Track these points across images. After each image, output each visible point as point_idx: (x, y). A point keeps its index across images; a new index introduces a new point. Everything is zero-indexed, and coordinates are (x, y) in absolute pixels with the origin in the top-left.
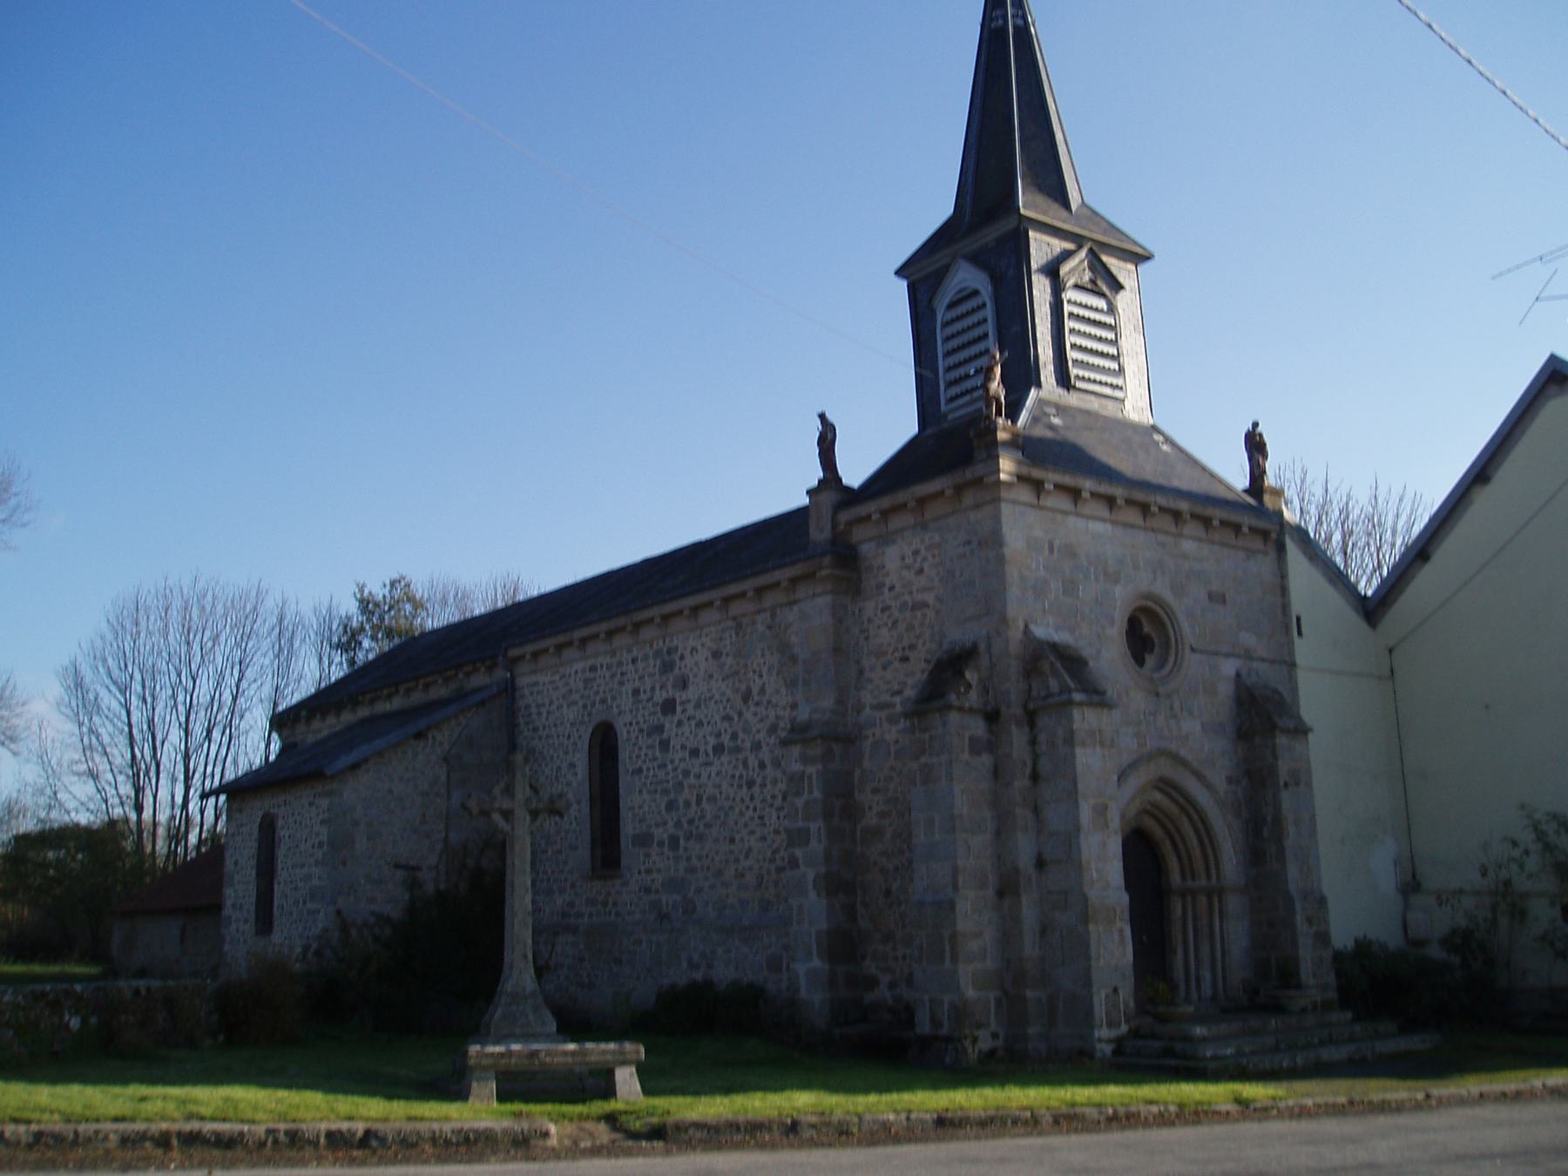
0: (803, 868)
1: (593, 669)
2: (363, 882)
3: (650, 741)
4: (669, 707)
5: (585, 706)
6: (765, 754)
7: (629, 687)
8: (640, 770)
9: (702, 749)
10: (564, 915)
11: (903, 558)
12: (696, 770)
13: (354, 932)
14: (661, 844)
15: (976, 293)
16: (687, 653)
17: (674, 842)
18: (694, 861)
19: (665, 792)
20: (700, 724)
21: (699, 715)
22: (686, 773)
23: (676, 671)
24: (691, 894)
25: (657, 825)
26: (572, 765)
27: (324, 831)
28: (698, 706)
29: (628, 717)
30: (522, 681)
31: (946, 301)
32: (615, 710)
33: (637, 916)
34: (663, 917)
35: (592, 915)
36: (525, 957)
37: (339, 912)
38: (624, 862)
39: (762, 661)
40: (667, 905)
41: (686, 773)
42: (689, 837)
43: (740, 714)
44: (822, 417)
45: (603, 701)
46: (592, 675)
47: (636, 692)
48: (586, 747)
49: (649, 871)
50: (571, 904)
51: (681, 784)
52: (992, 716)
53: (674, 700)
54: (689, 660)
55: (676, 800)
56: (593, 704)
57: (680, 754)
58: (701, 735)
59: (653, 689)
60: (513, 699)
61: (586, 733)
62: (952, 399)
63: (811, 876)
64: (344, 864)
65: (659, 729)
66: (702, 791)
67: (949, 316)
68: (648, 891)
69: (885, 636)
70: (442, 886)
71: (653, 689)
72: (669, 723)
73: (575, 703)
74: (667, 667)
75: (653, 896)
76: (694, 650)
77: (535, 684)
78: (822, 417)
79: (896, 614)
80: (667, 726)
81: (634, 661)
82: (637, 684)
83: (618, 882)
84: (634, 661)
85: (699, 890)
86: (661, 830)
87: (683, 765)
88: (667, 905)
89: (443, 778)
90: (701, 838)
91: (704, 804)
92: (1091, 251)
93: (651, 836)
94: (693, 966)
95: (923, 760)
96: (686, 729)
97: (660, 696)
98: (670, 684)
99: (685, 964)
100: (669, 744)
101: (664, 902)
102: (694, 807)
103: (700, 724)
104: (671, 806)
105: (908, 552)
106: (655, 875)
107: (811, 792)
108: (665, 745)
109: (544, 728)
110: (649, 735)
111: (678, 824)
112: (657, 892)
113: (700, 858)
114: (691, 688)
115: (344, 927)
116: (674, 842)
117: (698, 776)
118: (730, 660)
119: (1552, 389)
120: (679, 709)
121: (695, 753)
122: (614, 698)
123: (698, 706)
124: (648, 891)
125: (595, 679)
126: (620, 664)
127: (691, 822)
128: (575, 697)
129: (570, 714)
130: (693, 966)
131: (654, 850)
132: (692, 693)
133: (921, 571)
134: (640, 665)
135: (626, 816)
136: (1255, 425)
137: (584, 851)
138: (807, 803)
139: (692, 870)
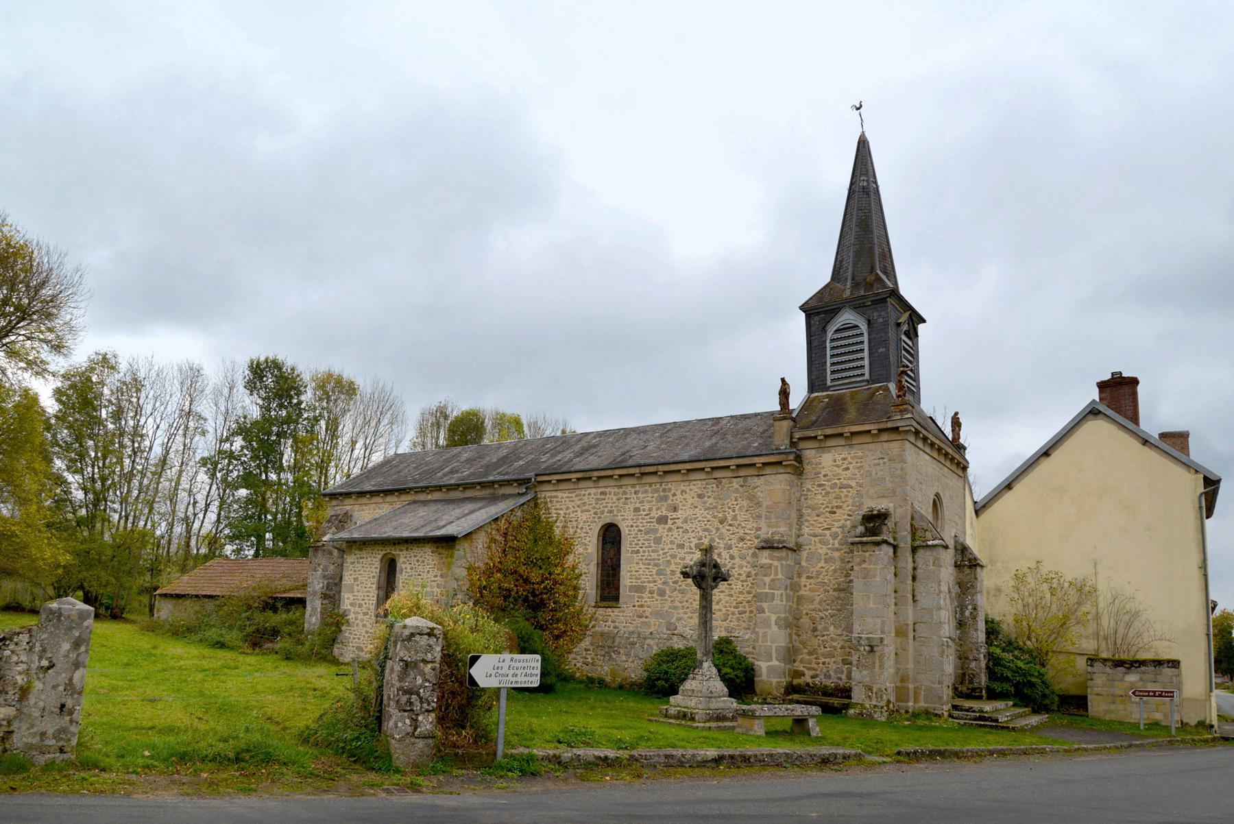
0: (767, 614)
4: (663, 520)
5: (595, 513)
6: (734, 551)
8: (638, 552)
9: (687, 544)
11: (835, 461)
12: (682, 555)
14: (651, 592)
15: (856, 327)
20: (686, 531)
21: (685, 526)
23: (670, 501)
28: (685, 521)
31: (835, 329)
39: (614, 500)
41: (673, 556)
43: (718, 529)
44: (783, 380)
45: (611, 512)
49: (642, 606)
56: (602, 513)
62: (833, 380)
63: (773, 618)
67: (836, 336)
69: (819, 499)
72: (661, 529)
78: (783, 380)
79: (828, 489)
92: (910, 315)
95: (863, 566)
96: (675, 533)
97: (656, 514)
103: (686, 531)
105: (839, 457)
107: (776, 574)
110: (646, 534)
118: (711, 500)
119: (1090, 417)
131: (646, 595)
133: (847, 469)
136: (956, 414)
138: (773, 580)
139: (675, 608)
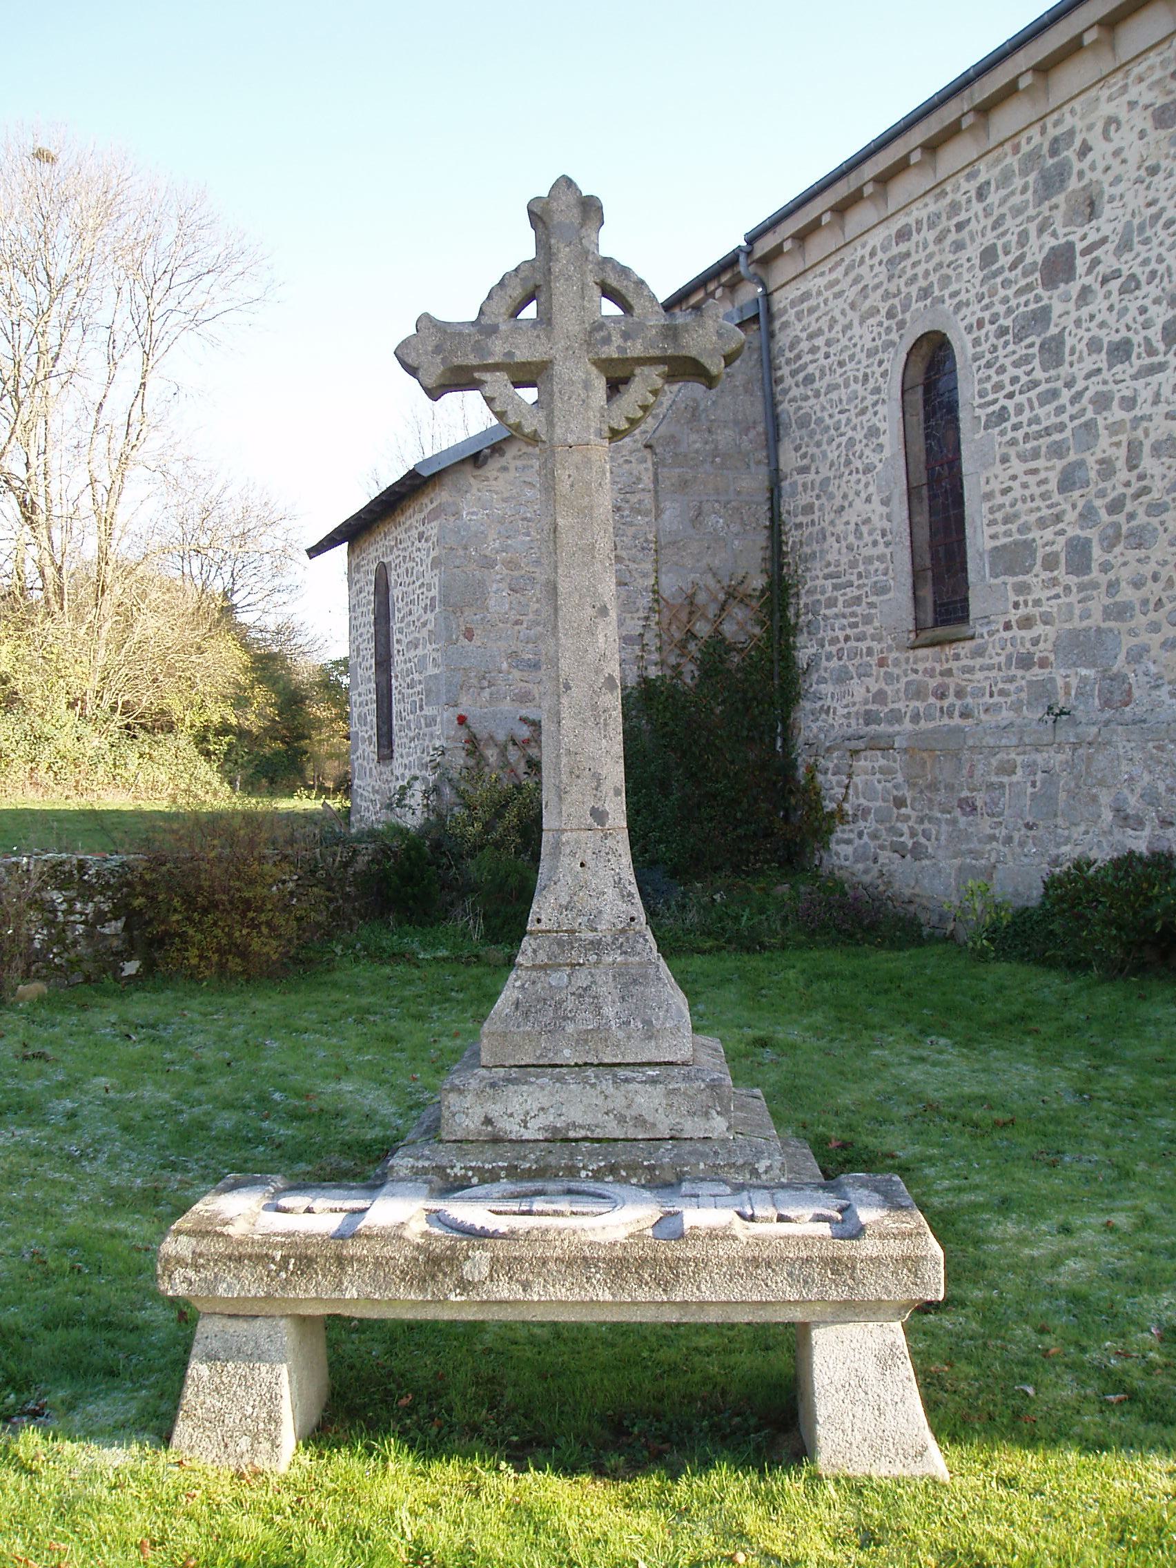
1: (903, 235)
2: (505, 666)
3: (1021, 351)
5: (890, 315)
7: (973, 251)
8: (1002, 415)
10: (870, 718)
13: (491, 754)
14: (1050, 563)
16: (1095, 138)
17: (1079, 555)
18: (1127, 594)
19: (1058, 450)
21: (1129, 265)
22: (1102, 402)
23: (1073, 184)
24: (1119, 665)
25: (1042, 523)
26: (873, 432)
27: (433, 578)
28: (1125, 246)
29: (974, 312)
30: (781, 300)
32: (949, 304)
33: (1006, 715)
34: (1059, 714)
35: (918, 714)
36: (599, 815)
37: (462, 720)
38: (975, 608)
40: (1067, 686)
41: (1102, 402)
42: (1110, 542)
45: (925, 293)
46: (903, 247)
47: (989, 255)
48: (897, 393)
49: (1027, 623)
50: (880, 697)
51: (1090, 426)
52: (870, 1006)
53: (1070, 246)
54: (1101, 149)
55: (1081, 464)
57: (1088, 364)
58: (1133, 307)
59: (1023, 238)
60: (771, 335)
61: (895, 362)
64: (469, 634)
65: (1041, 317)
66: (1140, 433)
68: (1025, 662)
70: (653, 672)
71: (1023, 238)
72: (1059, 302)
73: (874, 311)
74: (1052, 182)
75: (1037, 673)
76: (1112, 122)
77: (806, 296)
80: (1058, 308)
81: (981, 194)
82: (991, 236)
83: (964, 648)
84: (981, 194)
85: (1137, 655)
86: (1048, 534)
87: (1094, 386)
88: (1067, 686)
89: (647, 480)
90: (1139, 539)
91: (1148, 463)
93: (1028, 547)
94: (1124, 818)
96: (1098, 304)
97: (1036, 253)
98: (1058, 216)
99: (1108, 815)
100: (1063, 343)
101: (1060, 682)
102: (1123, 475)
104: (1067, 483)
106: (1039, 629)
108: (1053, 351)
109: (823, 374)
110: (1018, 339)
111: (1087, 516)
112: (1043, 663)
113: (1137, 584)
114: (1108, 211)
115: (473, 746)
116: (1079, 555)
117: (1129, 403)
120: (1081, 263)
121: (1121, 351)
122: (945, 281)
123: (1125, 246)
124: (1025, 662)
125: (907, 255)
126: (954, 208)
127: (1115, 506)
128: (874, 299)
129: (865, 335)
130: (1124, 818)
131: (1036, 577)
132: (1108, 223)
134: (993, 198)
135: (975, 510)
137: (899, 597)
139: (1120, 612)
